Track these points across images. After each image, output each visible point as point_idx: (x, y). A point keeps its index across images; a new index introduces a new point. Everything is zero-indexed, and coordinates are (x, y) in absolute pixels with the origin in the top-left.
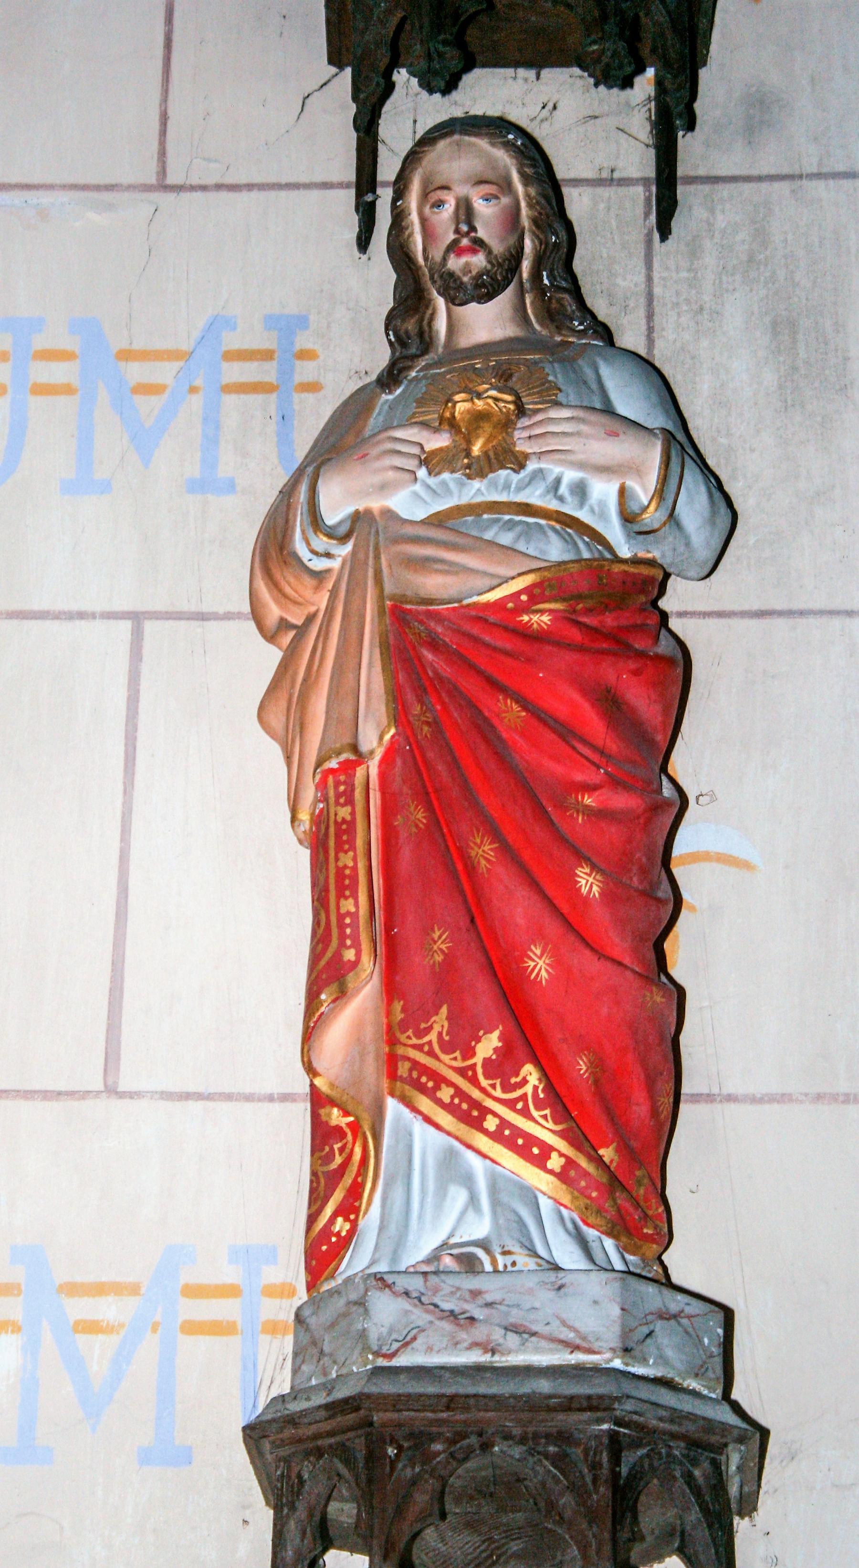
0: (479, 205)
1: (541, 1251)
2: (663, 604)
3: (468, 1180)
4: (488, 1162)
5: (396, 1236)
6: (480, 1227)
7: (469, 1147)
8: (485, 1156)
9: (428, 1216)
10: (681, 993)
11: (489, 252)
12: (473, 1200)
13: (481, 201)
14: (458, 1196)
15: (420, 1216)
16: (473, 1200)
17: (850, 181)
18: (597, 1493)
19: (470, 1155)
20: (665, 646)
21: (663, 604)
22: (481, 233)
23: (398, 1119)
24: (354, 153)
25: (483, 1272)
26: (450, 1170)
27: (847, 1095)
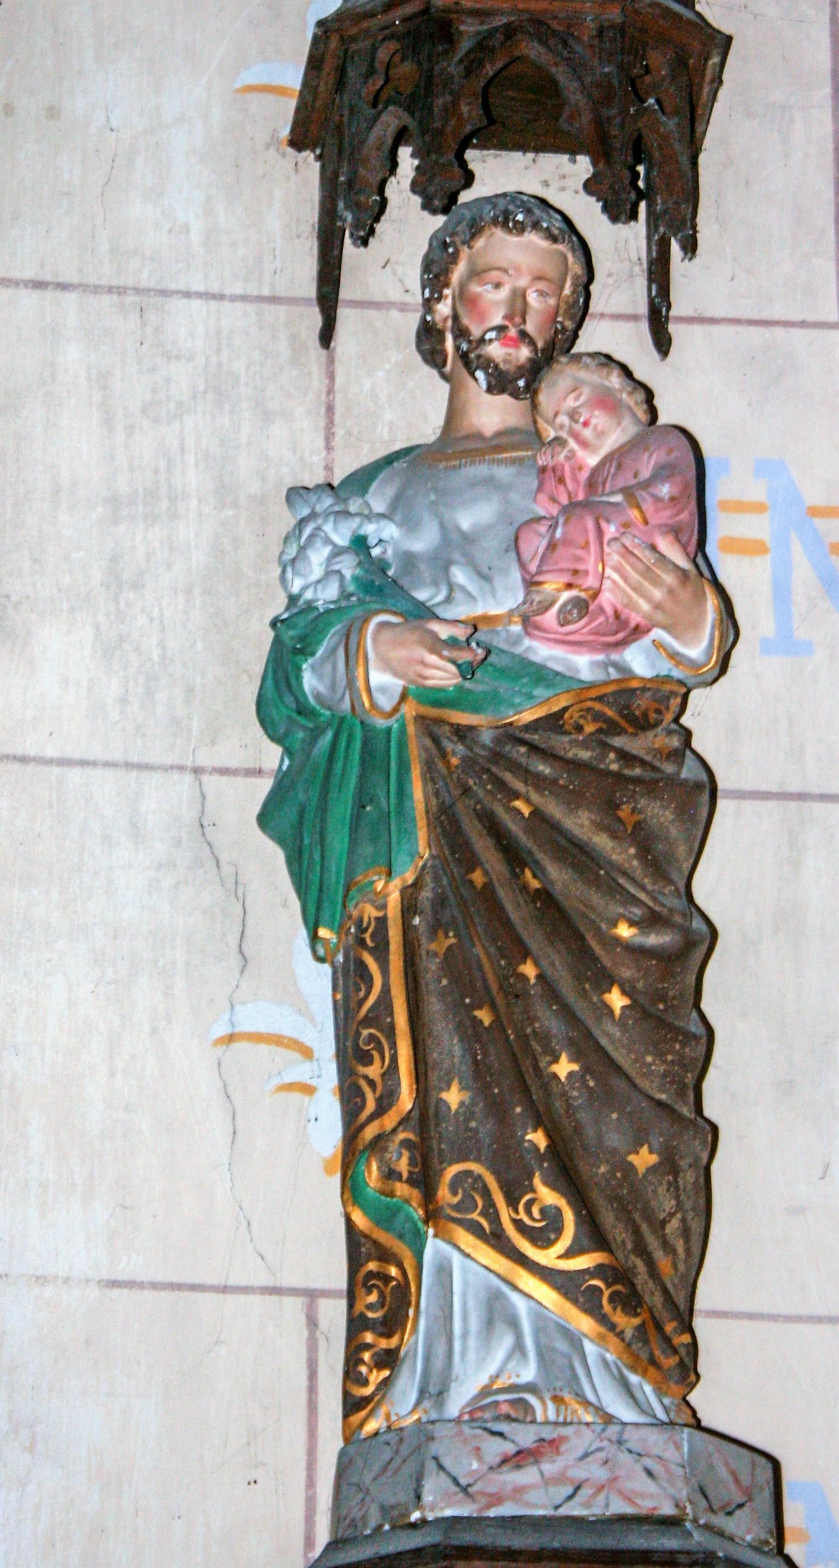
0: (532, 298)
1: (590, 1396)
2: (684, 720)
3: (513, 1323)
4: (532, 1303)
5: (435, 1392)
6: (528, 1373)
7: (515, 1288)
8: (529, 1297)
9: (471, 1355)
10: (715, 1129)
11: (532, 343)
12: (519, 1347)
13: (535, 295)
14: (505, 1342)
15: (464, 1353)
16: (519, 1347)
17: (286, 99)
18: (561, 323)
19: (515, 1297)
20: (689, 771)
21: (684, 720)
22: (530, 328)
23: (437, 1252)
24: (671, 278)
25: (533, 1421)
26: (496, 1313)
27: (726, 797)
